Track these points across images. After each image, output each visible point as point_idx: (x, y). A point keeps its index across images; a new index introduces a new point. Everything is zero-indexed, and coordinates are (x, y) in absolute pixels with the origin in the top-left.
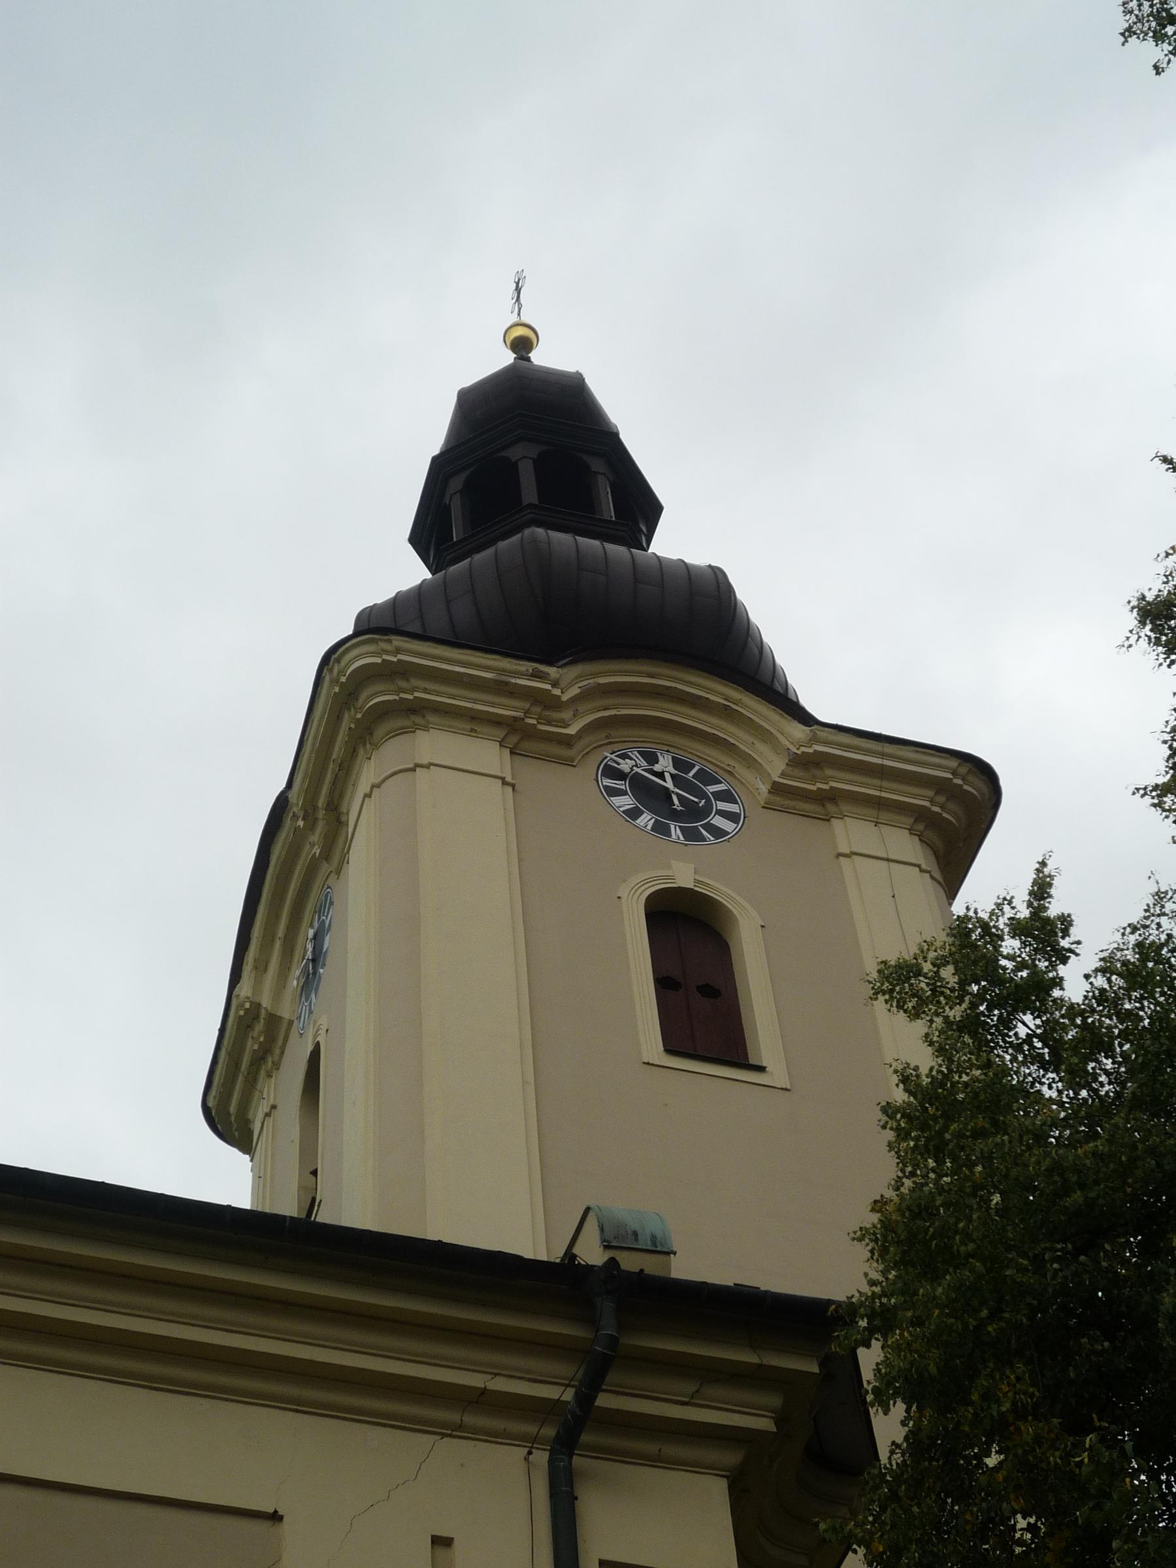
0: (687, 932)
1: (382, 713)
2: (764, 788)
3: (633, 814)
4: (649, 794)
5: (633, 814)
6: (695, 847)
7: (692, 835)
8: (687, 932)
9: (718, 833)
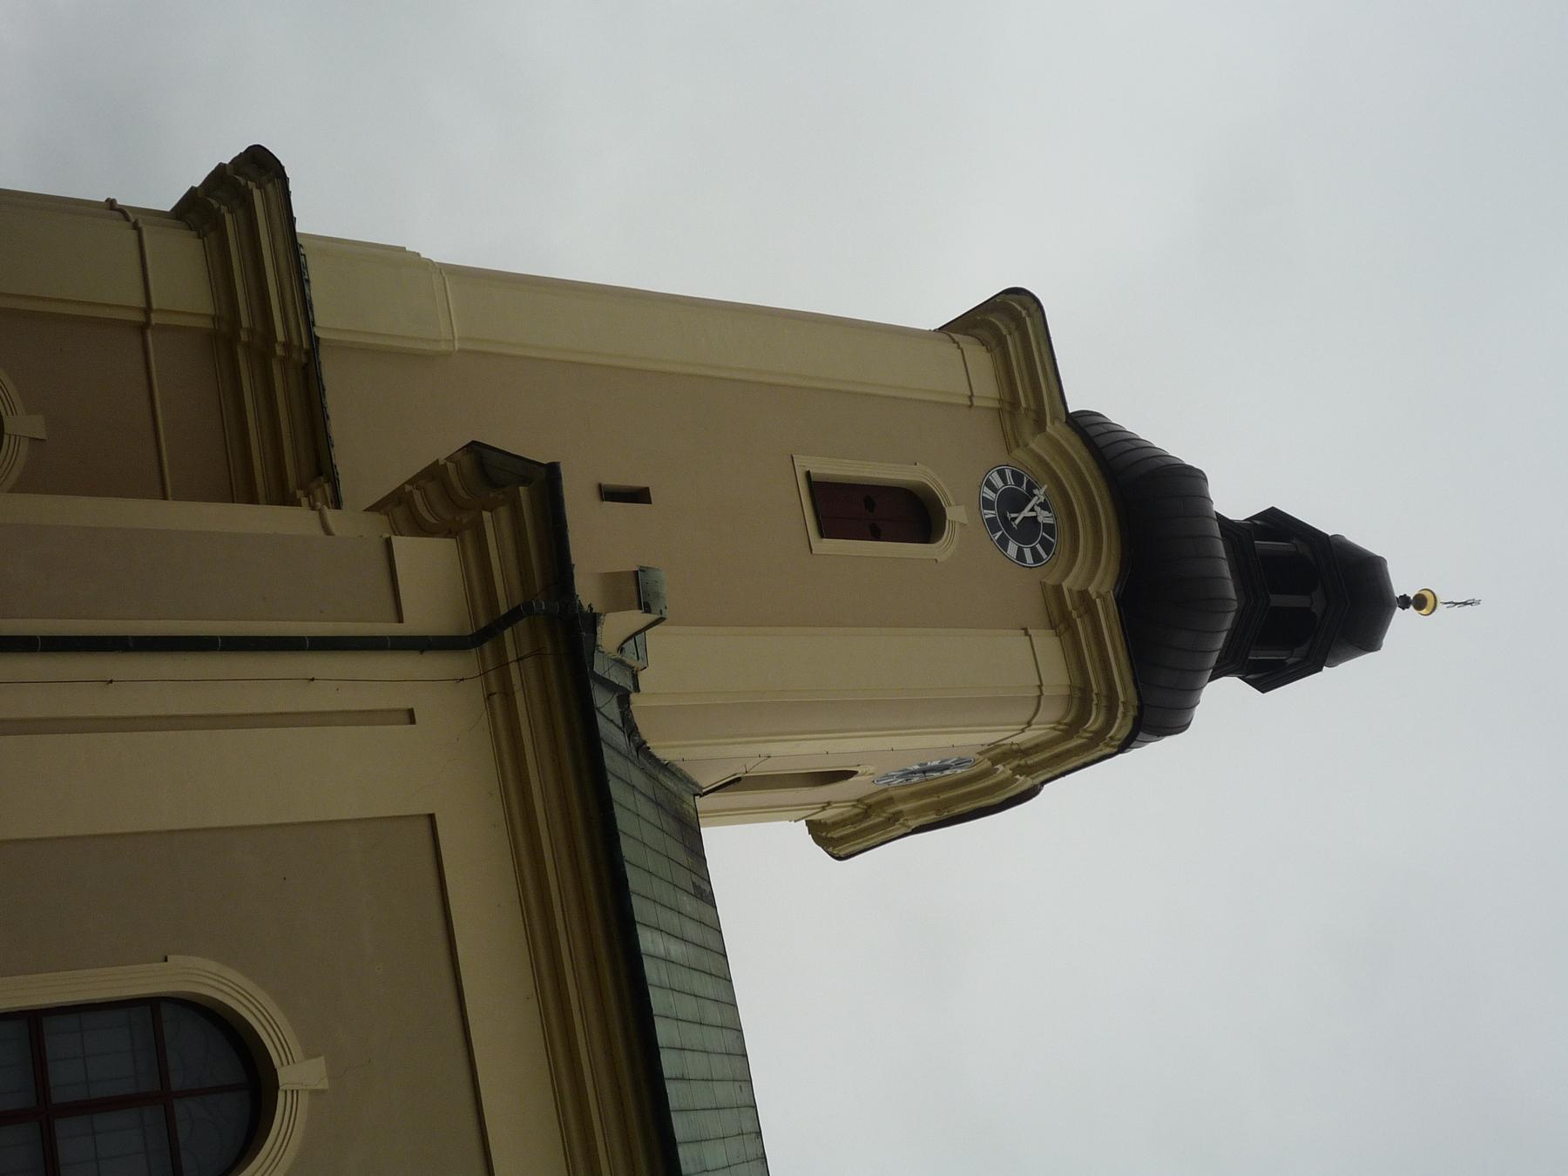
0: (908, 514)
3: (990, 485)
4: (1013, 500)
6: (983, 531)
7: (992, 525)
8: (908, 514)
9: (1003, 543)
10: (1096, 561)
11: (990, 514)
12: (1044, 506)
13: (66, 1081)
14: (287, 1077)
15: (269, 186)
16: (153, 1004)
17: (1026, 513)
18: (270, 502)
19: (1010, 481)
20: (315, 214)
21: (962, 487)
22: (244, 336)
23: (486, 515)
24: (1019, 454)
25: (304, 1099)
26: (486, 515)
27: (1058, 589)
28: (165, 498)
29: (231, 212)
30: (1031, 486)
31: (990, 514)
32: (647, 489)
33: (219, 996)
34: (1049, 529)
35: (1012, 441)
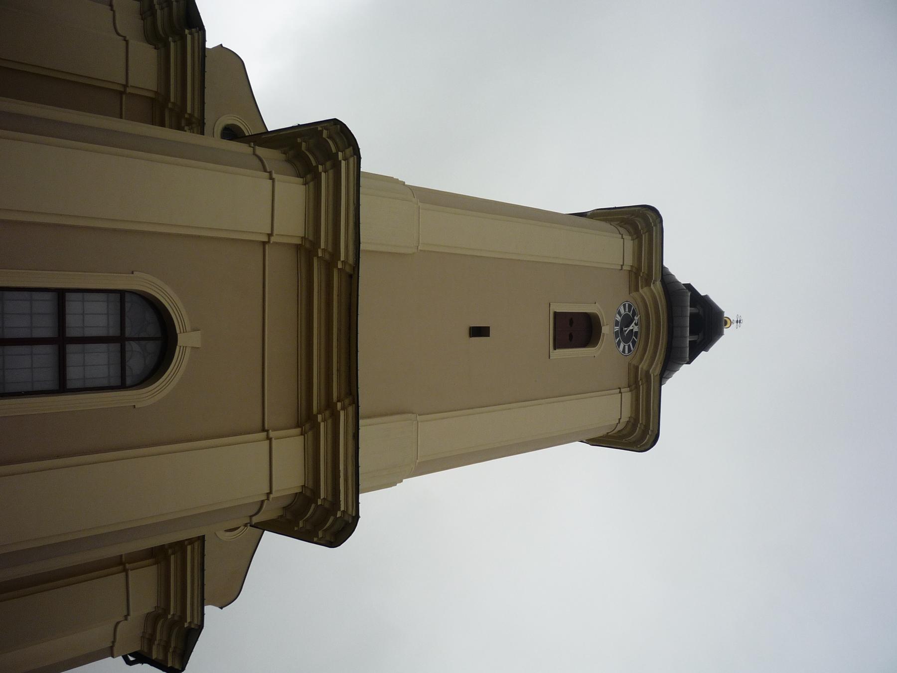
1: (635, 227)
2: (635, 362)
3: (619, 313)
4: (627, 321)
5: (619, 313)
6: (613, 336)
10: (655, 353)
11: (617, 328)
12: (636, 324)
13: (45, 355)
14: (182, 340)
15: (351, 160)
16: (122, 293)
17: (631, 328)
18: (171, 127)
19: (631, 314)
20: (371, 163)
21: (608, 310)
22: (170, 105)
23: (187, 31)
24: (634, 294)
25: (188, 351)
26: (187, 31)
27: (637, 368)
28: (121, 118)
29: (174, 42)
30: (634, 314)
31: (619, 318)
32: (489, 336)
33: (161, 380)
34: (636, 332)
35: (634, 287)
